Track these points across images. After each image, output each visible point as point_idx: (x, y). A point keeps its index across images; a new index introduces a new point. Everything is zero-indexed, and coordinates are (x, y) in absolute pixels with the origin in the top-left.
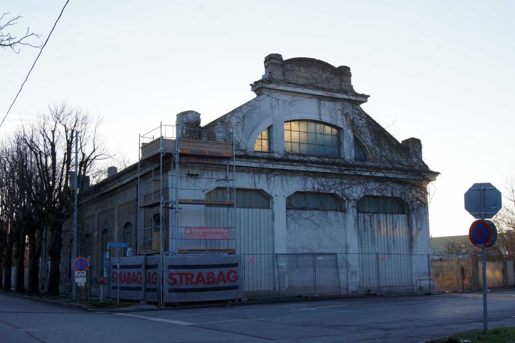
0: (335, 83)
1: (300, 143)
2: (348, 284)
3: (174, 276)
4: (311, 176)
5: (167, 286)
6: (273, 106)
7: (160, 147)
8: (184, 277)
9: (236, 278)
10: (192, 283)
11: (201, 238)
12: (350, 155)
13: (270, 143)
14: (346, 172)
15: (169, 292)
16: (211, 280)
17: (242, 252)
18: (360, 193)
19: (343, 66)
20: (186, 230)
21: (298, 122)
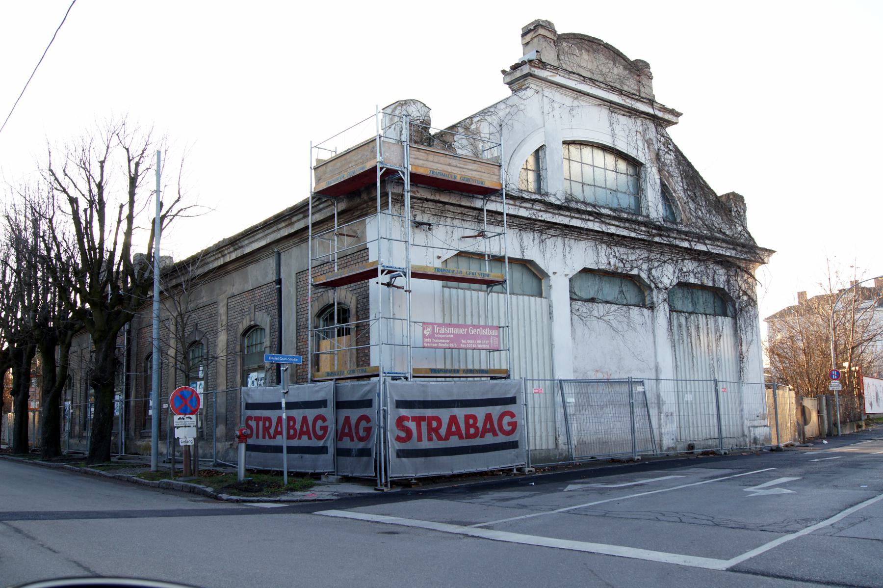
1: (583, 184)
3: (406, 423)
4: (605, 242)
5: (394, 446)
7: (375, 157)
8: (424, 425)
9: (514, 425)
10: (440, 438)
11: (452, 345)
13: (539, 178)
14: (657, 239)
15: (398, 456)
17: (523, 376)
21: (578, 147)
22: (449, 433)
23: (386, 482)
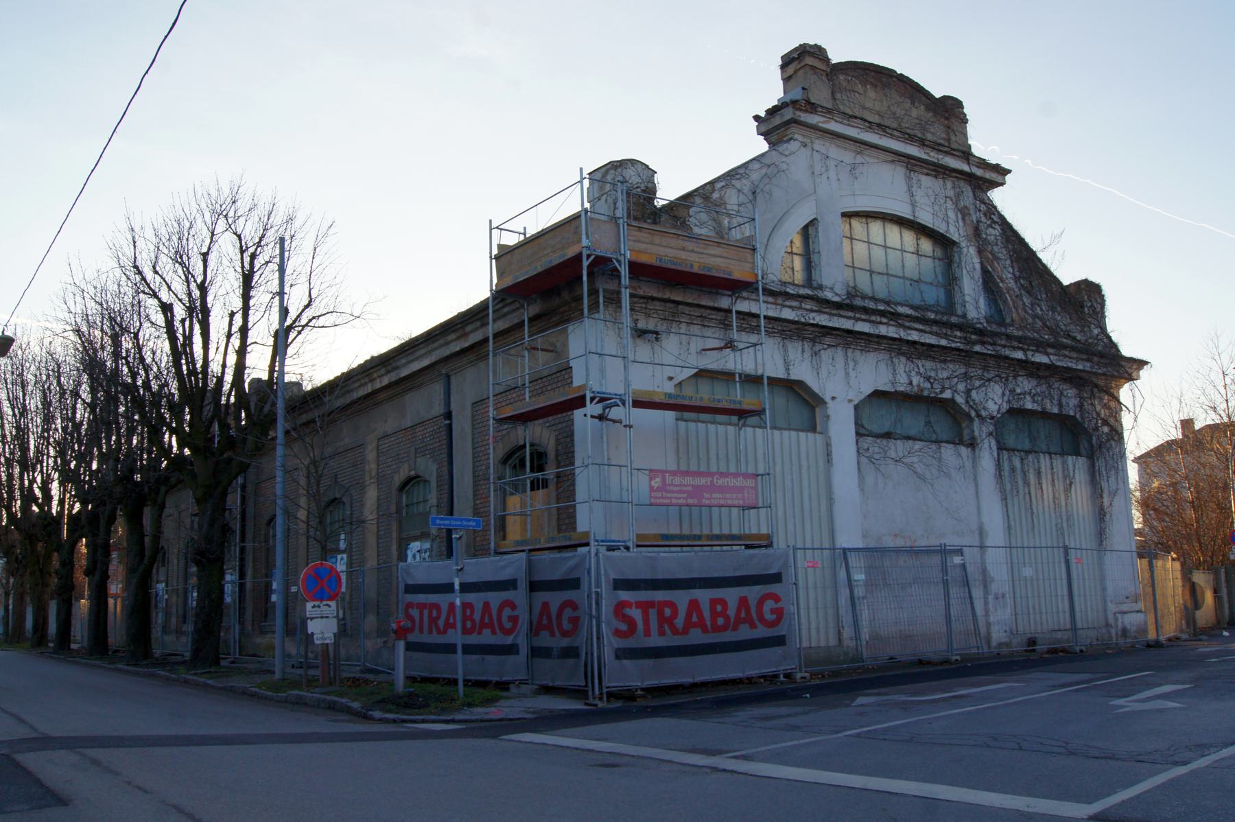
0: (936, 132)
1: (871, 272)
2: (988, 625)
4: (903, 354)
5: (611, 643)
6: (817, 172)
7: (580, 241)
8: (653, 613)
9: (779, 613)
10: (675, 632)
11: (690, 501)
12: (977, 308)
14: (977, 348)
15: (618, 657)
16: (721, 621)
18: (1000, 402)
19: (949, 97)
20: (651, 479)
22: (688, 625)
23: (601, 694)
